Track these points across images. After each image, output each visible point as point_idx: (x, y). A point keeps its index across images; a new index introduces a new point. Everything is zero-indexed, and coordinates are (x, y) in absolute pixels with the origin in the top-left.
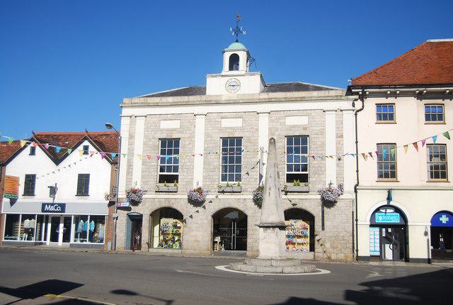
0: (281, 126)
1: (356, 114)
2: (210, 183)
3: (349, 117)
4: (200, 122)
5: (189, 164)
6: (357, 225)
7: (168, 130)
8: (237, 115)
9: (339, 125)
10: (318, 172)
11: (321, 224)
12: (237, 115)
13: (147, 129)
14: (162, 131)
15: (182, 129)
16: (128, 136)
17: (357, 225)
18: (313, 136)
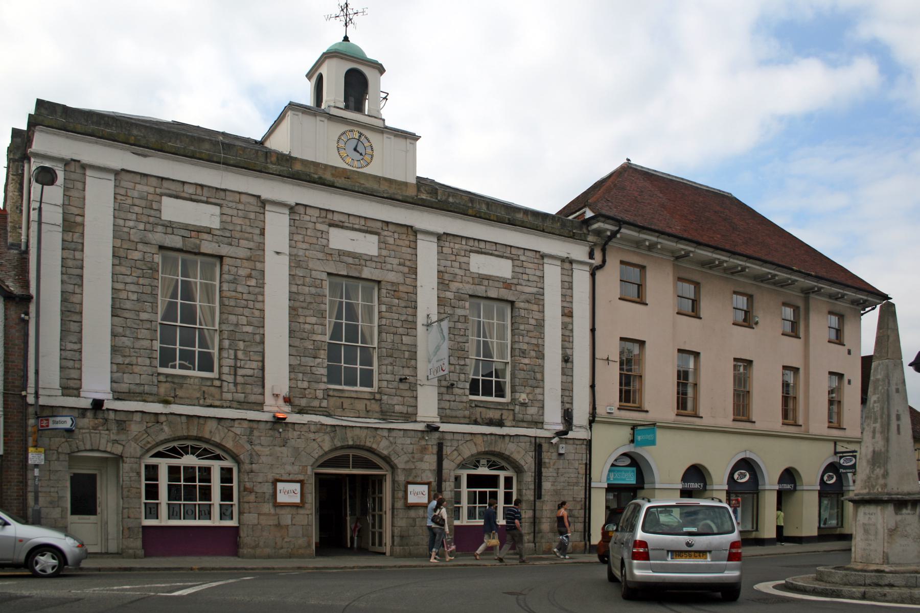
0: (461, 272)
1: (593, 275)
2: (305, 385)
3: (581, 277)
4: (277, 227)
5: (249, 329)
6: (40, 223)
7: (186, 227)
8: (366, 226)
9: (567, 287)
10: (531, 382)
11: (36, 239)
12: (366, 226)
13: (119, 210)
14: (170, 227)
15: (227, 234)
16: (59, 220)
17: (40, 223)
18: (522, 305)
